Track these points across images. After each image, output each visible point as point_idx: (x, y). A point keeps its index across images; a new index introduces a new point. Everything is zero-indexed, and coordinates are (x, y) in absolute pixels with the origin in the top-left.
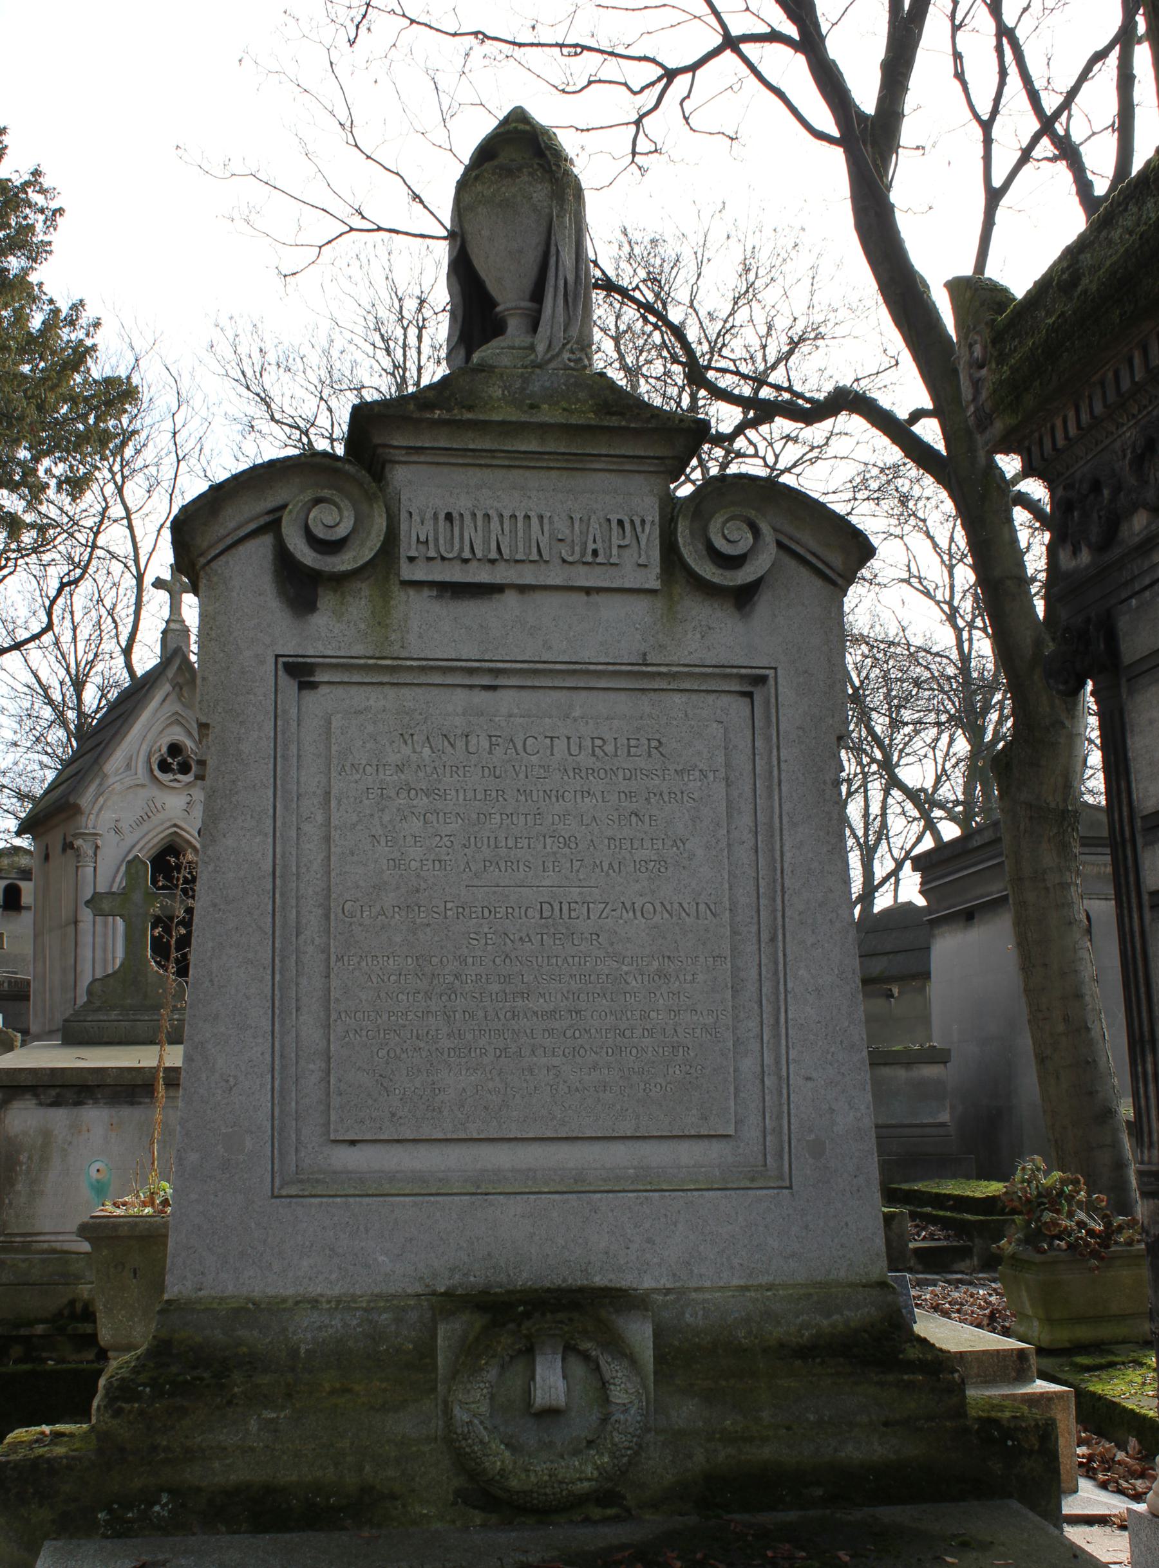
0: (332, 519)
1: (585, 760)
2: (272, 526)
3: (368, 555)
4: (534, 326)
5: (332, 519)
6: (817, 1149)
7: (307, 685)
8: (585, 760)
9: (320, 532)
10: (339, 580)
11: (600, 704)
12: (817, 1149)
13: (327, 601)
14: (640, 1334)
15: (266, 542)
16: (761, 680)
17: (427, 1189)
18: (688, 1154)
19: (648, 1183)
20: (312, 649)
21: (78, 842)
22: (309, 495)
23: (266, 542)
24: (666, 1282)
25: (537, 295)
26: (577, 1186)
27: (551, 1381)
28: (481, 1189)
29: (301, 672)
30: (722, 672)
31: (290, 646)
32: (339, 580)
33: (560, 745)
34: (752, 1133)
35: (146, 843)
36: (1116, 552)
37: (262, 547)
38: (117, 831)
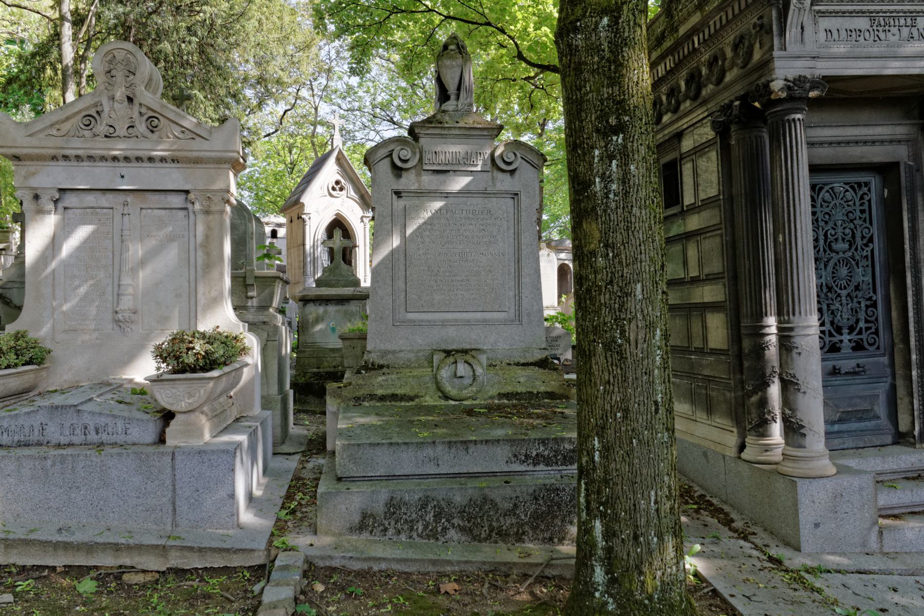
0: (406, 153)
1: (471, 216)
2: (390, 155)
3: (415, 163)
4: (458, 98)
5: (406, 153)
6: (529, 315)
7: (399, 197)
8: (471, 216)
9: (403, 158)
10: (407, 170)
11: (474, 201)
12: (529, 315)
13: (404, 174)
14: (483, 358)
15: (389, 159)
16: (517, 194)
17: (432, 324)
18: (496, 315)
19: (485, 322)
20: (400, 187)
21: (303, 216)
22: (399, 148)
23: (389, 159)
24: (490, 347)
25: (459, 89)
26: (468, 323)
27: (462, 369)
28: (444, 324)
29: (398, 194)
30: (157, 547)
31: (396, 187)
32: (407, 170)
33: (464, 212)
34: (512, 311)
35: (329, 218)
36: (721, 86)
37: (387, 161)
38: (317, 212)
